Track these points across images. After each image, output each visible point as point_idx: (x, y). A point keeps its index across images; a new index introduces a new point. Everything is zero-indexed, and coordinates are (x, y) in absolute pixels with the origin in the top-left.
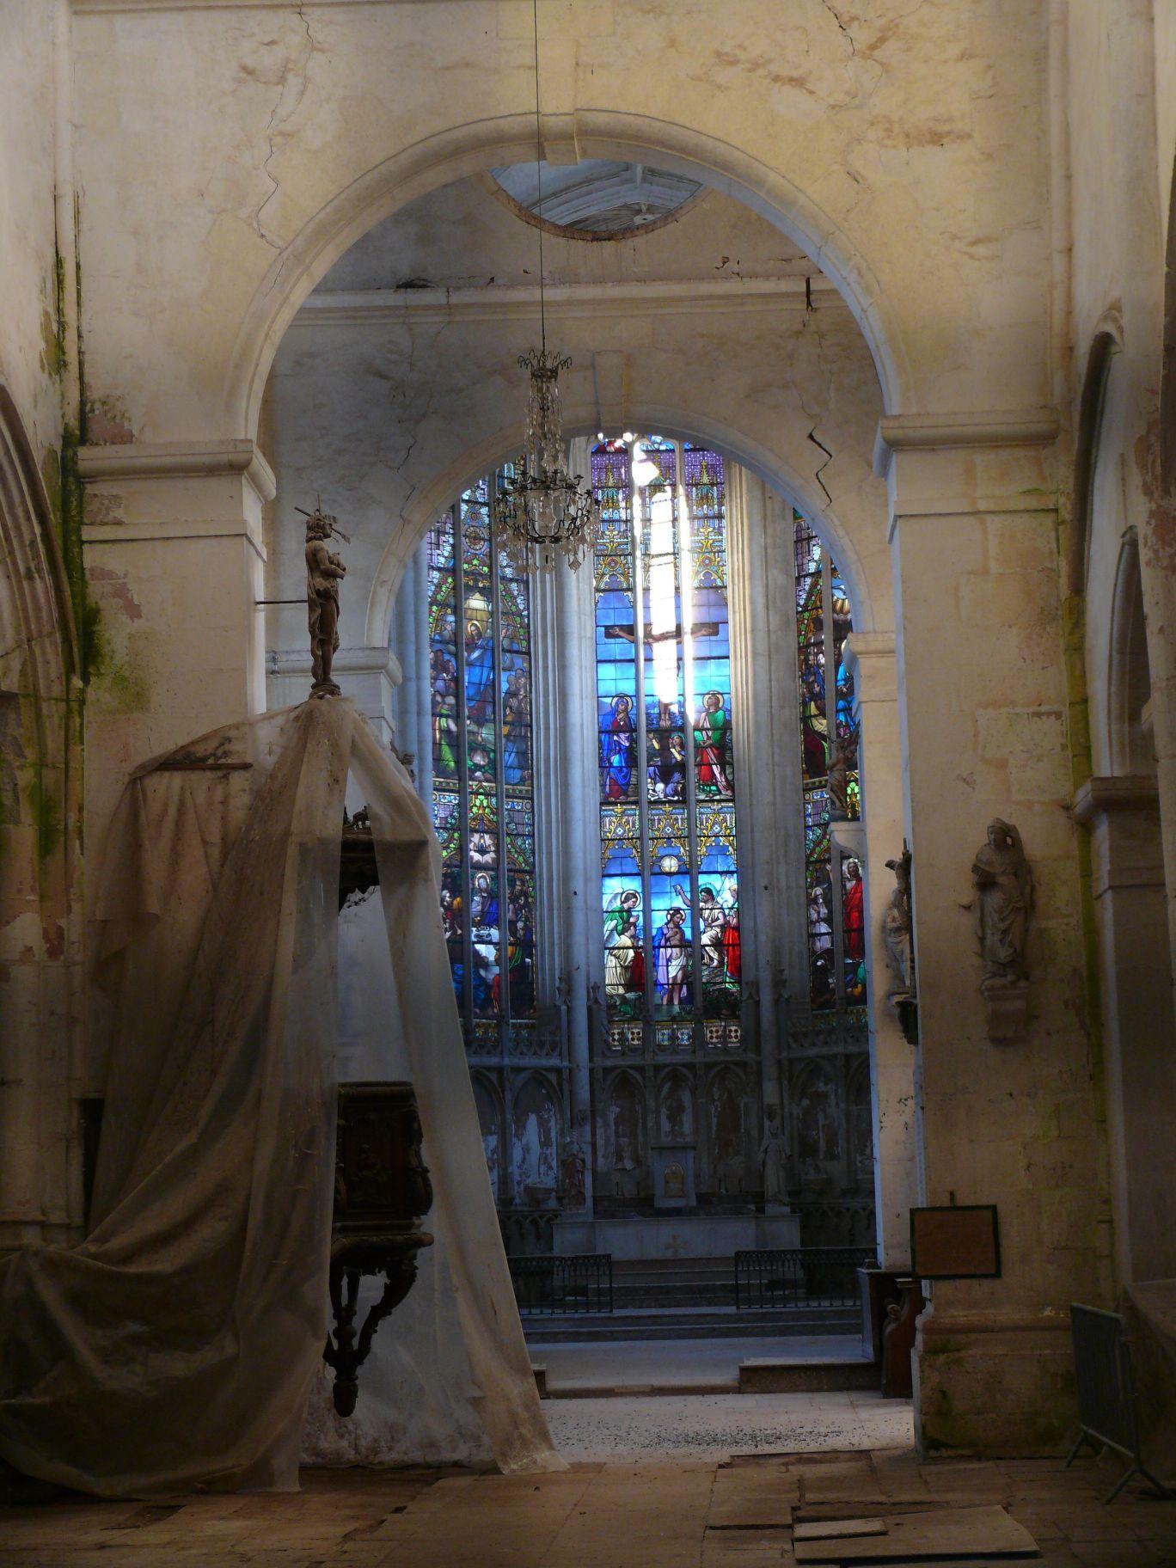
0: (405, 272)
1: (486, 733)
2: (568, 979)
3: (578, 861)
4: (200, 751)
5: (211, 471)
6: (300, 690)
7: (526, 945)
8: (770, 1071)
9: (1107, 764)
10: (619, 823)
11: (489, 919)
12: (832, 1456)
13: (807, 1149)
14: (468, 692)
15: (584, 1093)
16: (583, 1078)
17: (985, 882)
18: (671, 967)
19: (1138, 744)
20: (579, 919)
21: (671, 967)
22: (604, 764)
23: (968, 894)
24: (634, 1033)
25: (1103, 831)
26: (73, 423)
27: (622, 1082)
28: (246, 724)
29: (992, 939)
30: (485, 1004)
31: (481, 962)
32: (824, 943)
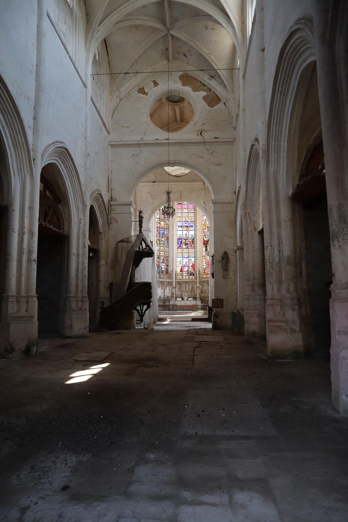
0: (153, 181)
1: (163, 239)
2: (173, 270)
3: (174, 255)
4: (125, 240)
5: (127, 205)
6: (138, 233)
7: (168, 266)
8: (198, 282)
9: (239, 244)
10: (180, 250)
11: (163, 262)
12: (203, 329)
13: (202, 292)
14: (161, 234)
15: (174, 285)
16: (174, 283)
17: (223, 258)
18: (186, 269)
19: (242, 242)
20: (174, 263)
21: (186, 269)
22: (178, 243)
23: (220, 259)
24: (181, 277)
25: (238, 252)
26: (110, 198)
27: (179, 283)
28: (130, 237)
29: (224, 266)
30: (162, 273)
31: (162, 268)
32: (205, 267)
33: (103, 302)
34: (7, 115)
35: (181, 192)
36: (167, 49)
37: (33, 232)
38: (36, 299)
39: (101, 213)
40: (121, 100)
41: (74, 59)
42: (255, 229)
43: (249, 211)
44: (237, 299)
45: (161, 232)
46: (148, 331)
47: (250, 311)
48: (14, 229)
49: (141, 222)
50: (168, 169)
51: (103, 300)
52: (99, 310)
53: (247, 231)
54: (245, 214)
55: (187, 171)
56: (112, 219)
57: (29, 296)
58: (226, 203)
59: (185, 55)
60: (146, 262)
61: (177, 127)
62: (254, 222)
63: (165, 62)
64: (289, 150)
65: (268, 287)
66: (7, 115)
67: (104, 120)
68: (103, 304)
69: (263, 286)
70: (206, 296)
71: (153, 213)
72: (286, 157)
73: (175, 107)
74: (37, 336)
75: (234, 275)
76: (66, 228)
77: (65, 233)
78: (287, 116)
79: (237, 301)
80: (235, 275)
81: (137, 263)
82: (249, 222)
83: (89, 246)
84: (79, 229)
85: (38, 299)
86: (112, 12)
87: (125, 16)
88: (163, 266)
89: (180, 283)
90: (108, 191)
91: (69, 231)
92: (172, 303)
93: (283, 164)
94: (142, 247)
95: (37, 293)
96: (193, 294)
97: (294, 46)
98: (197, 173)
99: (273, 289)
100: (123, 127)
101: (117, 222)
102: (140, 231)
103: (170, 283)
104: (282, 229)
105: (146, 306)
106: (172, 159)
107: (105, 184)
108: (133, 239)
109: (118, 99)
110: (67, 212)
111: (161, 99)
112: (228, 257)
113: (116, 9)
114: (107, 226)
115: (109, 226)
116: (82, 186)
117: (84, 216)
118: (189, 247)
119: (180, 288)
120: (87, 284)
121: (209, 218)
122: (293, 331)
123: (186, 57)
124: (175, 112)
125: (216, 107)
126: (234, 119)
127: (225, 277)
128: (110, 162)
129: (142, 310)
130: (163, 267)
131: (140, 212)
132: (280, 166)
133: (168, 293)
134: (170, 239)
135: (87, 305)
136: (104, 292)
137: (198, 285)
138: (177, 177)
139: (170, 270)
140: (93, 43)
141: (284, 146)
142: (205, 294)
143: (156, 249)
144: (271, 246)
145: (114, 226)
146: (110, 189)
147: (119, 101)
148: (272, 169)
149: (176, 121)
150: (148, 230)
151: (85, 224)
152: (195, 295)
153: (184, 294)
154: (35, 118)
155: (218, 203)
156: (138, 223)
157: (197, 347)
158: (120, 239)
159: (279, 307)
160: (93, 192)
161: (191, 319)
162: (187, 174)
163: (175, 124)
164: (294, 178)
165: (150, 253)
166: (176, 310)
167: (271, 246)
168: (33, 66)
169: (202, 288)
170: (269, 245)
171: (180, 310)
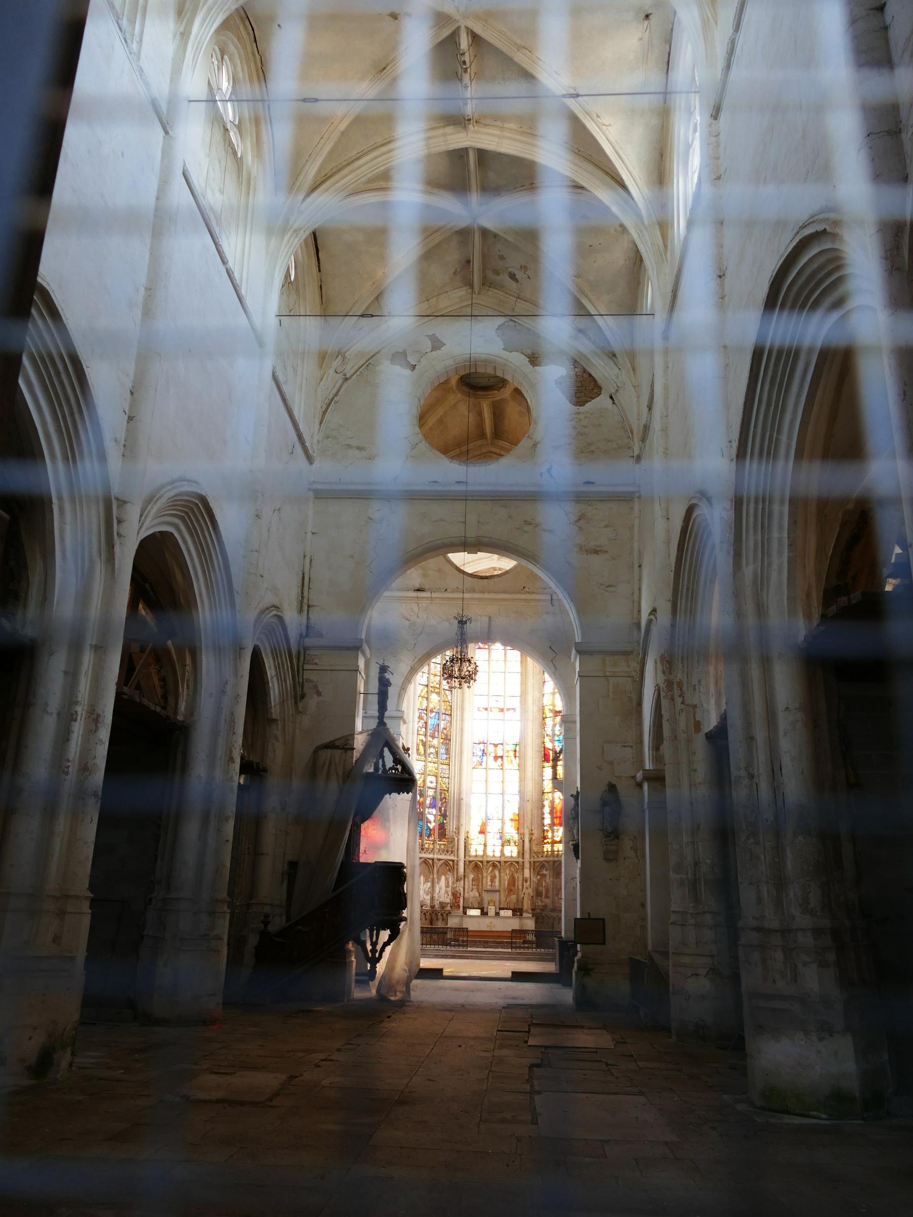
0: (417, 586)
1: (435, 742)
2: (458, 829)
4: (338, 743)
5: (348, 648)
7: (444, 816)
8: (527, 865)
11: (433, 806)
13: (538, 894)
14: (429, 727)
15: (461, 870)
16: (461, 865)
17: (604, 803)
19: (658, 758)
25: (646, 786)
26: (304, 628)
33: (267, 916)
34: (61, 406)
35: (490, 618)
36: (468, 262)
37: (98, 716)
38: (86, 907)
39: (278, 668)
40: (346, 379)
41: (237, 275)
42: (698, 726)
43: (679, 676)
44: (644, 919)
45: (431, 722)
46: (388, 1006)
47: (686, 960)
48: (46, 704)
50: (458, 558)
51: (267, 909)
52: (253, 940)
53: (674, 730)
54: (669, 684)
55: (506, 564)
56: (306, 685)
57: (67, 897)
58: (613, 653)
59: (513, 276)
60: (397, 803)
61: (484, 450)
62: (695, 706)
63: (463, 292)
64: (793, 522)
65: (747, 895)
66: (61, 406)
67: (301, 427)
68: (266, 923)
69: (726, 884)
70: (550, 906)
71: (413, 671)
72: (786, 542)
73: (482, 401)
74: (76, 1017)
75: (635, 849)
76: (182, 707)
77: (180, 718)
78: (790, 437)
79: (644, 927)
80: (639, 850)
81: (366, 811)
82: (679, 706)
83: (242, 758)
84: (219, 709)
85: (94, 903)
86: (339, 171)
87: (370, 181)
89: (476, 866)
90: (301, 610)
91: (192, 714)
92: (453, 922)
93: (780, 560)
94: (384, 765)
95: (92, 887)
96: (514, 897)
97: (808, 271)
98: (536, 570)
99: (759, 900)
100: (349, 446)
101: (319, 694)
102: (381, 723)
103: (450, 866)
104: (781, 733)
105: (388, 932)
106: (472, 534)
107: (295, 592)
109: (340, 377)
110: (188, 661)
111: (447, 382)
112: (618, 801)
113: (348, 164)
114: (290, 702)
115: (296, 702)
116: (236, 596)
117: (236, 674)
118: (506, 765)
119: (477, 881)
120: (228, 865)
121: (566, 692)
122: (826, 1030)
123: (517, 281)
124: (480, 414)
125: (588, 405)
126: (637, 437)
127: (611, 857)
128: (309, 535)
129: (374, 944)
130: (431, 818)
132: (769, 565)
133: (442, 891)
134: (453, 742)
135: (223, 927)
136: (269, 886)
137: (527, 873)
138: (482, 578)
139: (451, 827)
140: (286, 238)
141: (781, 514)
142: (548, 901)
143: (417, 765)
144: (752, 777)
145: (312, 702)
146: (304, 605)
147: (340, 382)
148: (748, 571)
149: (482, 435)
150: (400, 718)
151: (237, 697)
152: (520, 901)
153: (487, 897)
154: (130, 419)
155: (591, 653)
156: (374, 699)
157: (538, 1066)
158: (326, 739)
159: (779, 955)
160: (262, 612)
161: (509, 975)
162: (507, 572)
163: (479, 443)
164: (808, 595)
165: (404, 781)
166: (465, 944)
167: (752, 777)
168: (137, 290)
169: (539, 883)
170: (743, 773)
171: (475, 944)
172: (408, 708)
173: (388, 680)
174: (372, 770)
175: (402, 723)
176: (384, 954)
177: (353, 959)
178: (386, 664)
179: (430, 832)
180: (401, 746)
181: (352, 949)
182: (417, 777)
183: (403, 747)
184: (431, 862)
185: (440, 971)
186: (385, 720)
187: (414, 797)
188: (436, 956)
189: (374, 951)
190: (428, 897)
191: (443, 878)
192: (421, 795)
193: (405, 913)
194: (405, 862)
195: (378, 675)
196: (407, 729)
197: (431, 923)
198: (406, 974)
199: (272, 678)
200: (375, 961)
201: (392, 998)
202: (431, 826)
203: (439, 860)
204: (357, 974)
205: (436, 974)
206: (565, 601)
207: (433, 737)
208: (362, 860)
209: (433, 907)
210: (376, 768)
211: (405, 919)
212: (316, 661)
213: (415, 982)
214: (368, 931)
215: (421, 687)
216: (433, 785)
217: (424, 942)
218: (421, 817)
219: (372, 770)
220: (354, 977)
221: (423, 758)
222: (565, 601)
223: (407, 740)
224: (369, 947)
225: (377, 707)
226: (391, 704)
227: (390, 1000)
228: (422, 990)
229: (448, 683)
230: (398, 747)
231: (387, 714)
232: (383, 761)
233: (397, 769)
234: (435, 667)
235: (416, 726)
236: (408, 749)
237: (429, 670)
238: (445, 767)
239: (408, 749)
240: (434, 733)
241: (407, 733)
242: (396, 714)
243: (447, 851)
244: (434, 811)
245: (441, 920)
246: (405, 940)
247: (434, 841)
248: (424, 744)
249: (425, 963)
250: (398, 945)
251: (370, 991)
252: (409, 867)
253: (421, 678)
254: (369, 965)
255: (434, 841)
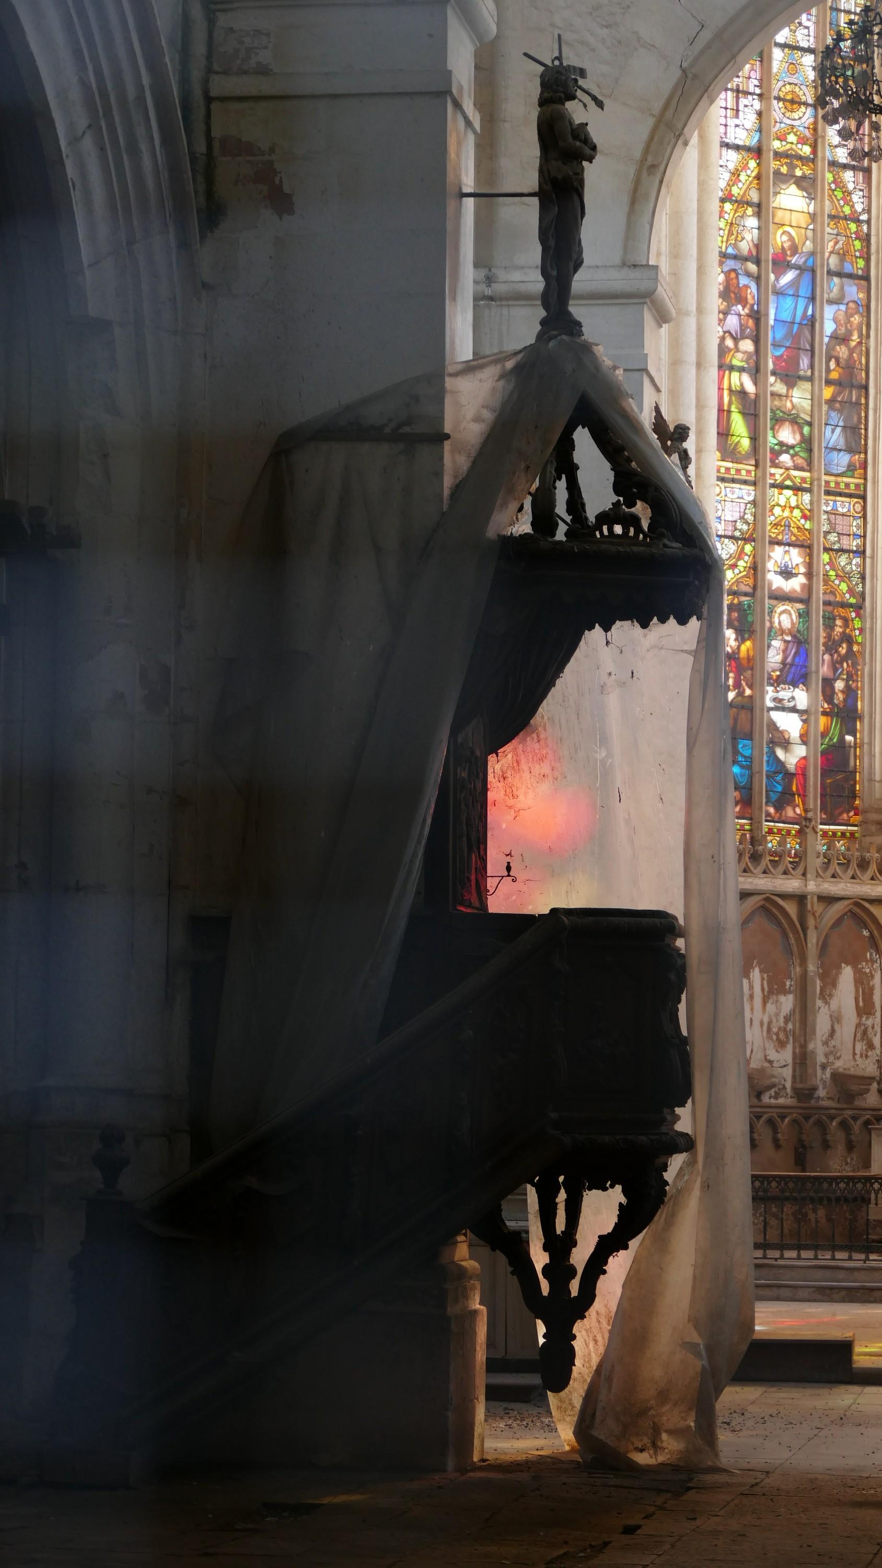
1: (800, 398)
7: (847, 715)
11: (795, 673)
14: (773, 333)
30: (783, 800)
49: (561, 194)
60: (627, 680)
71: (693, 87)
81: (510, 699)
88: (791, 718)
94: (576, 504)
105: (616, 1195)
108: (470, 405)
129: (559, 1246)
130: (790, 724)
131: (558, 86)
143: (721, 505)
150: (642, 297)
156: (526, 216)
165: (654, 564)
172: (676, 254)
173: (580, 133)
174: (524, 526)
175: (648, 318)
176: (603, 1284)
177: (476, 1304)
178: (571, 59)
179: (787, 785)
180: (646, 419)
181: (471, 1265)
182: (724, 550)
183: (660, 424)
184: (791, 908)
185: (844, 1348)
186: (576, 310)
187: (710, 641)
188: (826, 1294)
189: (559, 1269)
190: (787, 1055)
191: (847, 974)
192: (744, 631)
193: (685, 1120)
194: (677, 910)
195: (534, 114)
196: (676, 345)
197: (800, 1161)
198: (699, 1364)
199: (75, 141)
200: (566, 1311)
201: (643, 1458)
202: (792, 757)
203: (828, 900)
204: (492, 1366)
205: (827, 1362)
206: (859, 1312)
207: (790, 378)
208: (502, 900)
209: (804, 1094)
210: (544, 519)
211: (686, 1144)
212: (265, 57)
213: (733, 1396)
214: (532, 1194)
215: (732, 158)
216: (796, 584)
217: (773, 1236)
218: (745, 723)
219: (524, 526)
220: (481, 1380)
221: (746, 469)
222: (859, 1312)
223: (675, 395)
224: (540, 1259)
225: (535, 253)
226: (597, 233)
227: (633, 1467)
228: (765, 1431)
229: (845, 134)
230: (635, 426)
231: (581, 281)
232: (574, 488)
233: (634, 521)
234: (793, 67)
235: (714, 333)
236: (682, 433)
237: (765, 80)
238: (844, 505)
239: (682, 433)
240: (794, 362)
241: (676, 362)
242: (618, 280)
243: (863, 865)
244: (801, 698)
245: (841, 1148)
246: (686, 1231)
247: (804, 823)
248: (752, 409)
249: (774, 1320)
250: (662, 1244)
251: (552, 1429)
252: (695, 928)
253: (729, 119)
254: (541, 1329)
255: (804, 823)
